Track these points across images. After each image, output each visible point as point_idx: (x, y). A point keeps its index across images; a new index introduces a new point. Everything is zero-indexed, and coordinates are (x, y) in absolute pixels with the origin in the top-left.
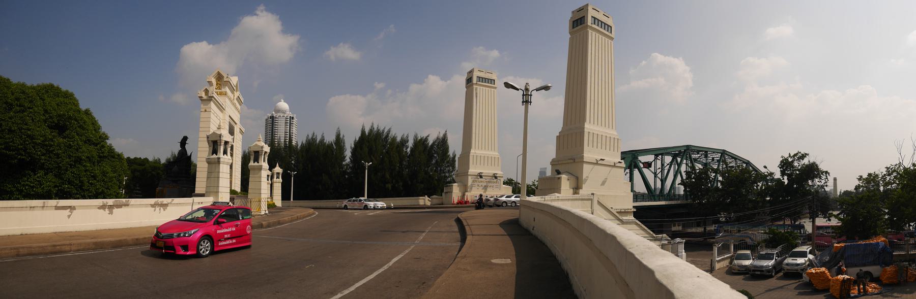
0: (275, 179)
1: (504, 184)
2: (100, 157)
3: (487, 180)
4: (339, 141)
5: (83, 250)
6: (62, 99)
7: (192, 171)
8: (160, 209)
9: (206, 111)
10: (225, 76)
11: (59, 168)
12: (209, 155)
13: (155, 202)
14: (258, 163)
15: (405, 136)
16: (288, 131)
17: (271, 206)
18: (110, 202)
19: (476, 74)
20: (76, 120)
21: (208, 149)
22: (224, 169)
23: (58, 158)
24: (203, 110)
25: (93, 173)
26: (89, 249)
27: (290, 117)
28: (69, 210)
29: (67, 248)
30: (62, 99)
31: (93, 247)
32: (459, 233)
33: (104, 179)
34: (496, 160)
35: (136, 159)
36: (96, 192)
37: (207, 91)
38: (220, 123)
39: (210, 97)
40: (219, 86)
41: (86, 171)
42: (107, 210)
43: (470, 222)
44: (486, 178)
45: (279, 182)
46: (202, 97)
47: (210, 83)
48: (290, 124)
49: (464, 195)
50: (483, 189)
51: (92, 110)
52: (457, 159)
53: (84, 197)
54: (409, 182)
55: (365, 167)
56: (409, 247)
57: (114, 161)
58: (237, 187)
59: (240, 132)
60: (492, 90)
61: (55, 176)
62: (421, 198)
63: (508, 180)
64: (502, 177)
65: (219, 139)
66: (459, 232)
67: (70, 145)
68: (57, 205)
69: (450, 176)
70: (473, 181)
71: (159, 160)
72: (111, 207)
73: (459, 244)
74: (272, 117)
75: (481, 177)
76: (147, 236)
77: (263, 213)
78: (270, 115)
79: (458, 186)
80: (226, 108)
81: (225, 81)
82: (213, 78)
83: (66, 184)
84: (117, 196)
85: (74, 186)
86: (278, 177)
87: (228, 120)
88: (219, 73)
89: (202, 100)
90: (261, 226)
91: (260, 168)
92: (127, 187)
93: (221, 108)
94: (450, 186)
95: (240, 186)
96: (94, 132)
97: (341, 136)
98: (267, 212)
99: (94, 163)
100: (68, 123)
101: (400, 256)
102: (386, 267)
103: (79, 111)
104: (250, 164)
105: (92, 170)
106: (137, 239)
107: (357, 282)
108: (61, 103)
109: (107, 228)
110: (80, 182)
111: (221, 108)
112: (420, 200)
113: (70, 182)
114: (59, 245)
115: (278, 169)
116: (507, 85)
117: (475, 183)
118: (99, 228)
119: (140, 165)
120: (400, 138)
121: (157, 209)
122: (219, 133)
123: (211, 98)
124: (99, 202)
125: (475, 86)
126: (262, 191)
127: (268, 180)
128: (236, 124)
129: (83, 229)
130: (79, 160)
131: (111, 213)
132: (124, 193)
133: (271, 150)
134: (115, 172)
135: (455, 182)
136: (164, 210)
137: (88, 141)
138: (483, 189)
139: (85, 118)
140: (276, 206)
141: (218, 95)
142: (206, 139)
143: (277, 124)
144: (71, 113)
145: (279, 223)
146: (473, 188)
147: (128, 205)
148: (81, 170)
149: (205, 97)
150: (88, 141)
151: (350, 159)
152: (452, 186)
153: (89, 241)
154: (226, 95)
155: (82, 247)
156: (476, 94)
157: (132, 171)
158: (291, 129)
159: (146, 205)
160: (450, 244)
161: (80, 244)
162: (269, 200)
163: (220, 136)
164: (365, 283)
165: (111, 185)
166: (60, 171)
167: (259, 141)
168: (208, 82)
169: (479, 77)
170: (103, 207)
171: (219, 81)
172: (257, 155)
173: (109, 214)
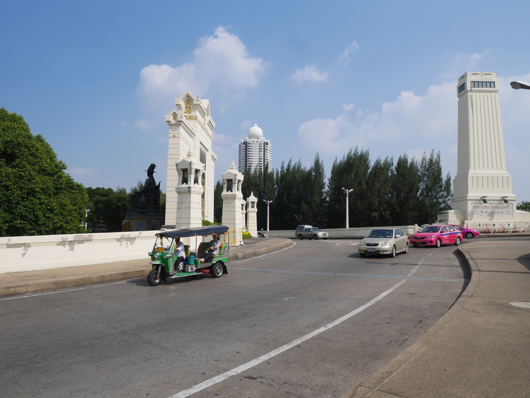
0: (250, 209)
1: (517, 209)
2: (57, 189)
3: (494, 205)
4: (318, 167)
5: (42, 291)
6: (9, 124)
7: (161, 202)
8: (127, 243)
9: (174, 136)
10: (195, 99)
11: (9, 201)
12: (178, 185)
13: (121, 236)
14: (232, 191)
15: (389, 159)
16: (263, 158)
17: (246, 237)
18: (70, 237)
19: (470, 78)
20: (26, 147)
21: (177, 178)
22: (195, 199)
23: (7, 190)
24: (172, 136)
25: (49, 206)
26: (48, 290)
27: (264, 142)
28: (23, 248)
29: (23, 290)
30: (9, 124)
31: (53, 286)
32: (461, 268)
33: (62, 213)
34: (505, 180)
35: (98, 189)
36: (54, 226)
37: (175, 115)
38: (190, 150)
39: (178, 121)
40: (189, 109)
41: (41, 204)
42: (67, 246)
43: (474, 255)
44: (492, 202)
45: (254, 212)
46: (170, 122)
47: (178, 106)
48: (265, 150)
49: (463, 223)
50: (488, 216)
51: (44, 137)
52: (452, 182)
53: (40, 233)
54: (398, 210)
55: (346, 194)
56: (400, 280)
57: (74, 193)
58: (211, 218)
59: (212, 159)
60: (493, 94)
61: (5, 211)
62: (410, 226)
63: (524, 204)
64: (515, 200)
65: (189, 167)
66: (461, 266)
67: (21, 175)
68: (8, 242)
69: (444, 202)
70: (475, 207)
71: (125, 190)
72: (71, 243)
73: (462, 280)
74: (245, 143)
75: (485, 201)
76: (113, 273)
77: (238, 244)
78: (243, 141)
79: (455, 213)
80: (197, 133)
81: (194, 105)
82: (181, 101)
83: (18, 220)
84: (79, 231)
85: (28, 221)
86: (253, 207)
87: (199, 147)
88: (188, 96)
89: (170, 125)
90: (236, 258)
91: (234, 198)
92: (89, 220)
93: (191, 133)
94: (444, 213)
95: (213, 217)
96: (49, 161)
97: (320, 162)
98: (242, 243)
99: (50, 195)
100: (18, 151)
101: (390, 291)
102: (373, 302)
103: (30, 137)
104: (223, 193)
105: (48, 202)
106: (102, 277)
107: (342, 315)
108: (8, 128)
109: (68, 265)
110: (34, 217)
111: (191, 133)
112: (409, 230)
113: (22, 217)
114: (13, 287)
115: (253, 198)
116: (515, 85)
117: (477, 209)
118: (59, 266)
119: (103, 195)
120: (384, 160)
121: (124, 243)
122: (189, 160)
123: (179, 123)
124: (58, 237)
125: (469, 94)
126: (237, 222)
127: (242, 209)
128: (207, 150)
129: (40, 268)
130: (32, 193)
131: (72, 249)
132: (86, 226)
133: (245, 178)
134: (75, 205)
135: (451, 209)
136: (132, 244)
137: (42, 171)
138: (488, 216)
139: (39, 145)
140: (251, 237)
141: (187, 119)
142: (175, 167)
143: (251, 150)
144: (20, 140)
145: (255, 254)
146: (475, 216)
147: (91, 240)
148: (35, 203)
149: (173, 122)
150: (42, 171)
151: (328, 186)
152: (448, 213)
153: (47, 280)
154: (196, 119)
155: (40, 288)
156: (472, 102)
157: (94, 203)
158: (266, 156)
159: (111, 240)
160: (450, 280)
161: (38, 285)
162: (244, 230)
163: (190, 164)
164: (351, 317)
165: (71, 220)
166: (10, 205)
167: (231, 169)
168: (177, 105)
169: (474, 82)
170: (62, 243)
171: (188, 104)
172: (230, 183)
173: (70, 250)
